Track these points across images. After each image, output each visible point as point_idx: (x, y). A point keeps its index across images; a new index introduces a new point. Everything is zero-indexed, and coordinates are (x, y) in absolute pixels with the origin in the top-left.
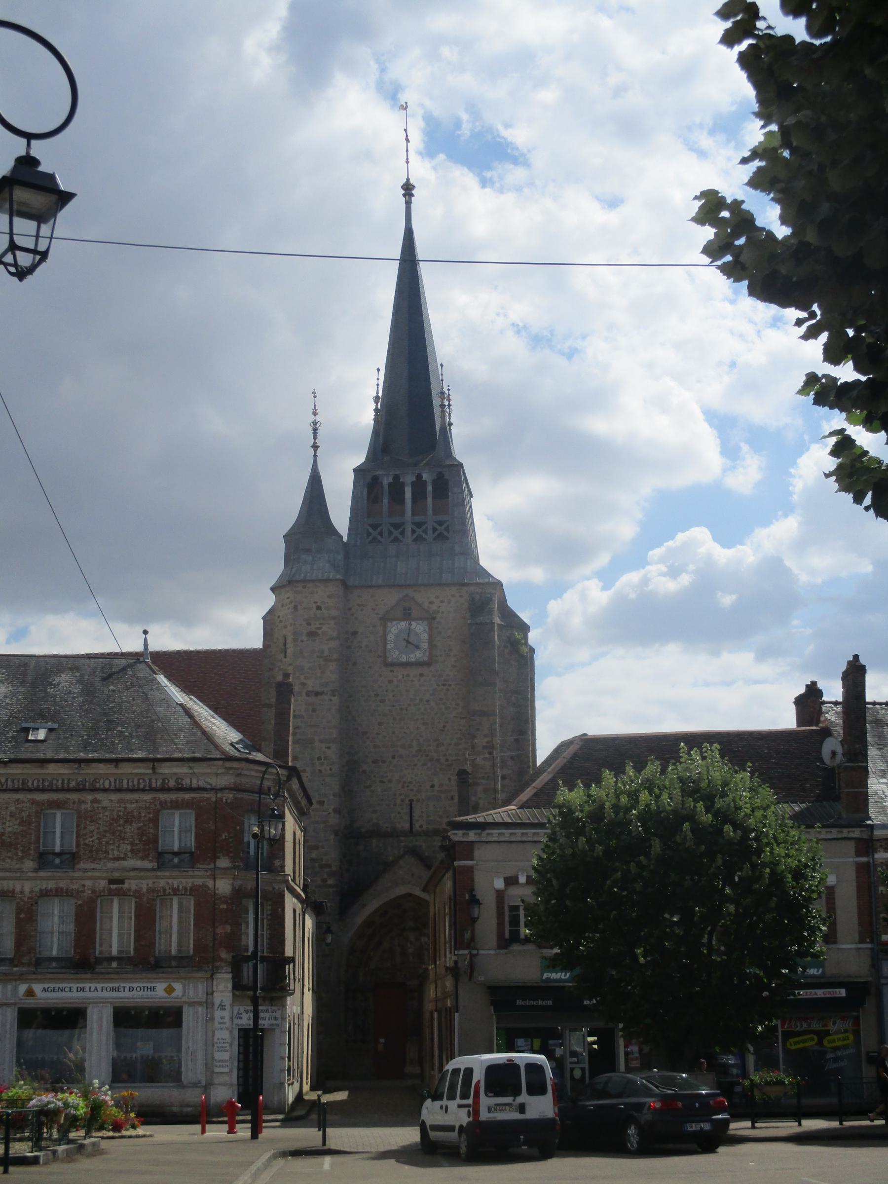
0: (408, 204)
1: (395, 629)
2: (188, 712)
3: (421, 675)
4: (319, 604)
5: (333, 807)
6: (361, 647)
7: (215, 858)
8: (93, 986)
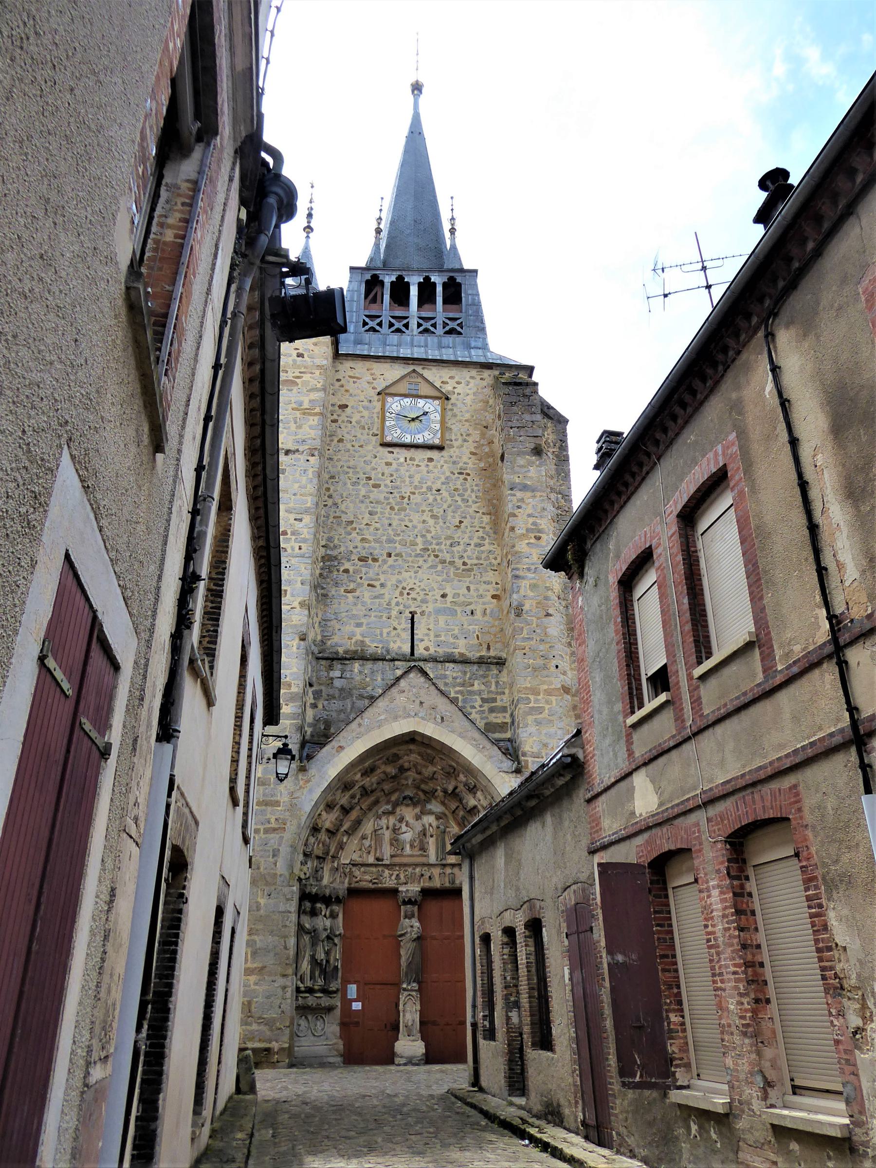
3: (431, 460)
4: (300, 351)
5: (300, 599)
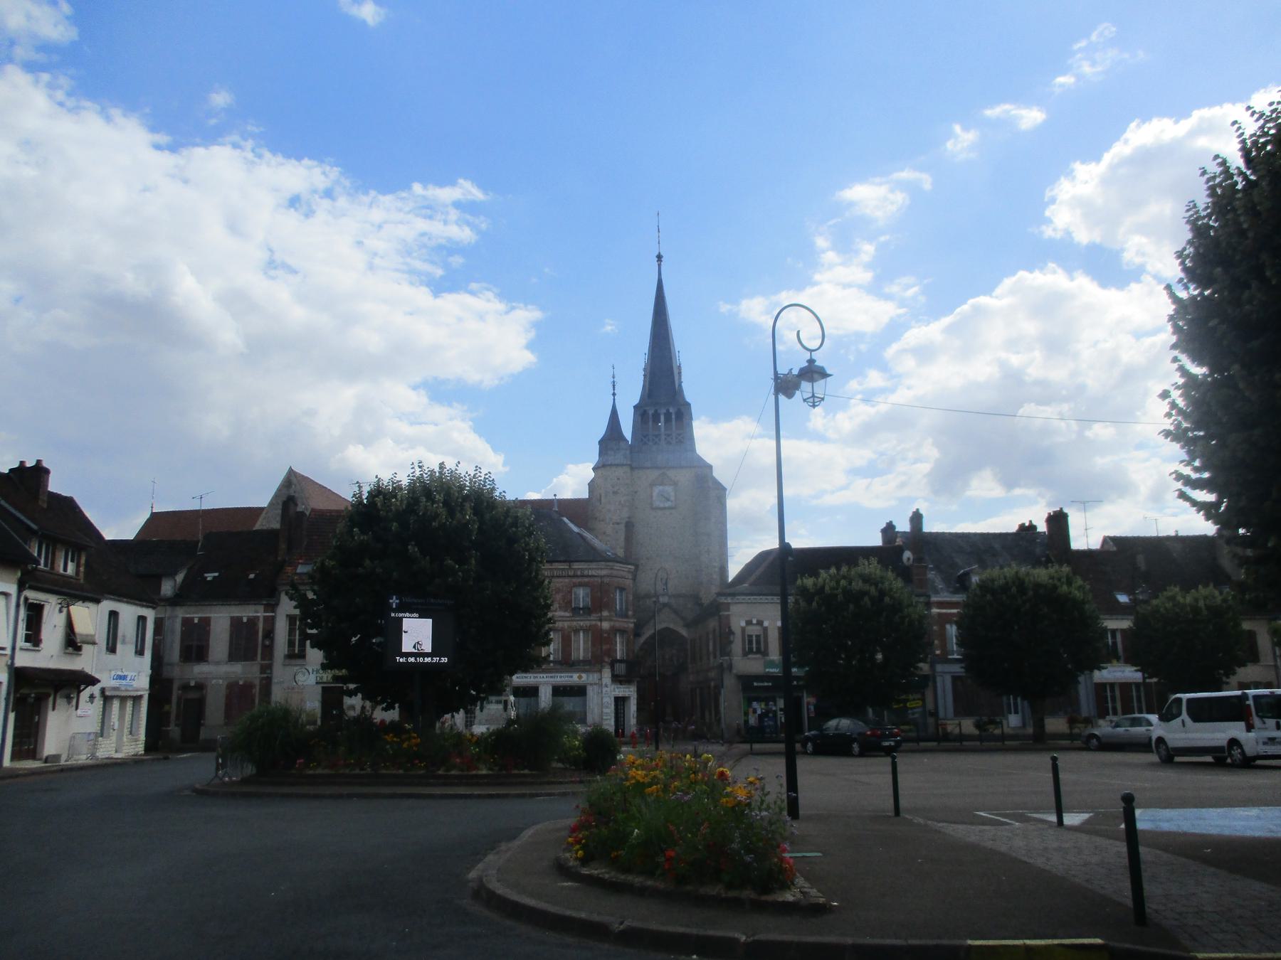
0: (659, 266)
1: (656, 490)
2: (582, 537)
3: (671, 514)
7: (601, 611)
8: (541, 675)
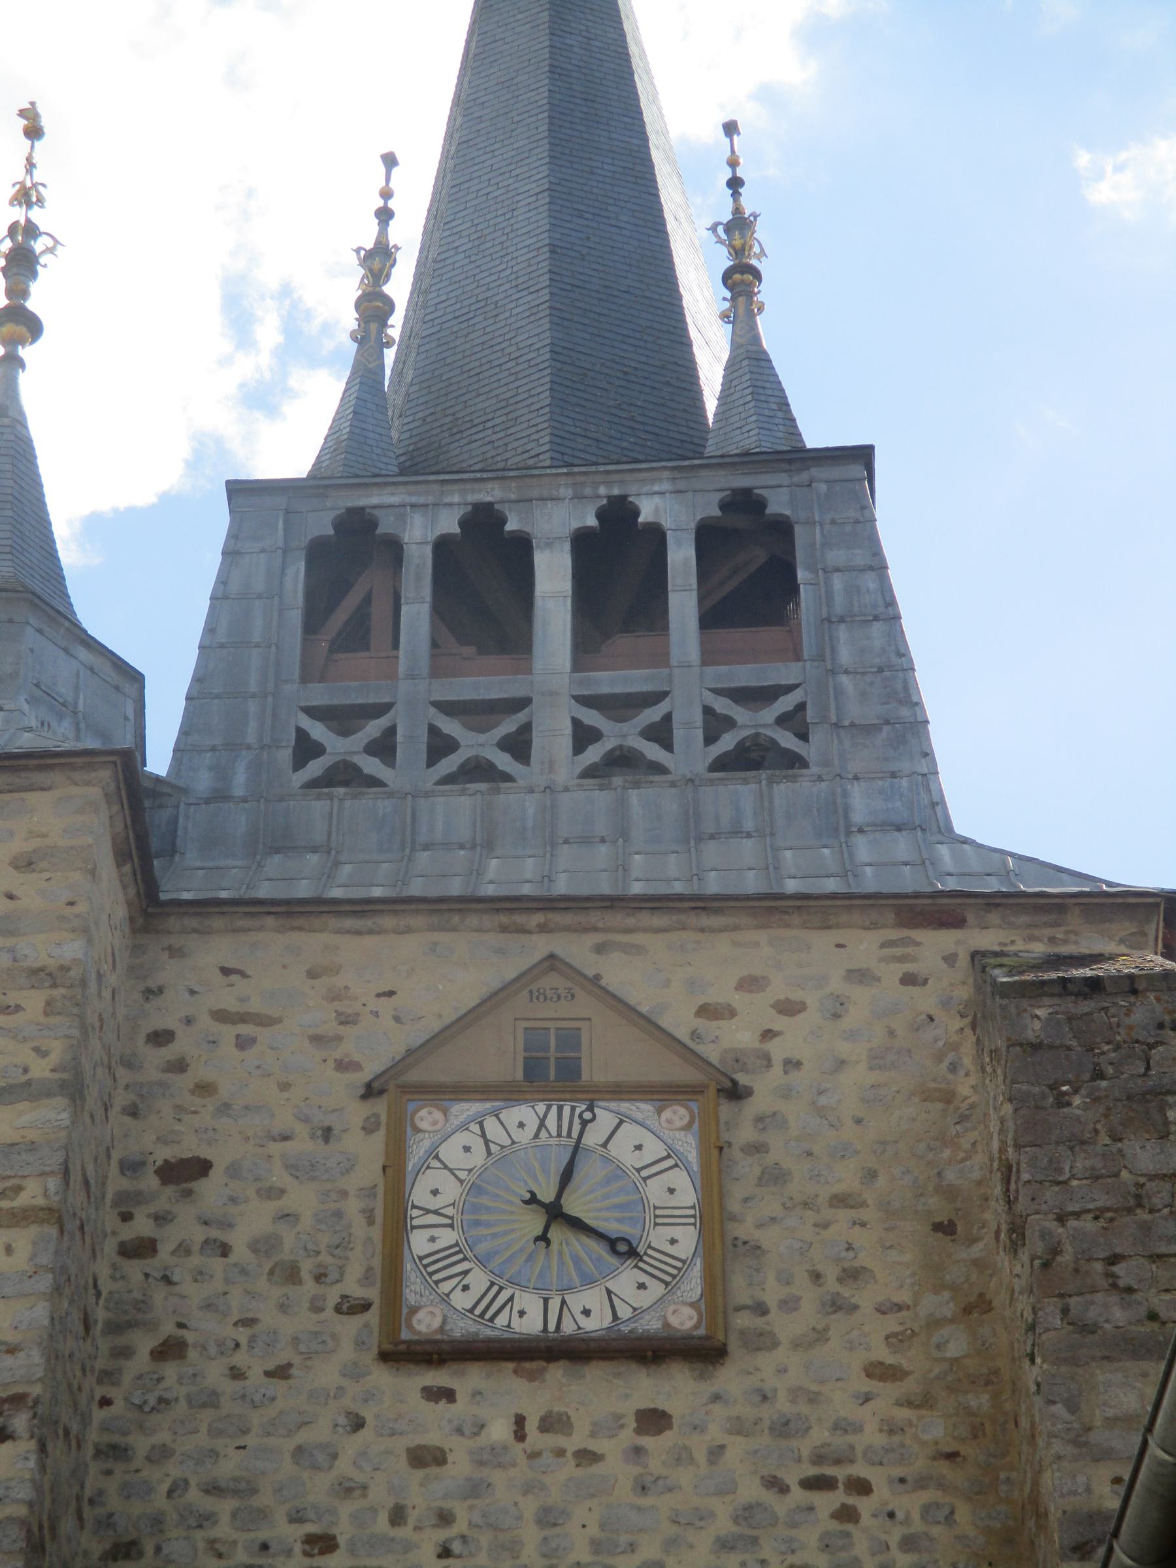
6: (225, 1250)
